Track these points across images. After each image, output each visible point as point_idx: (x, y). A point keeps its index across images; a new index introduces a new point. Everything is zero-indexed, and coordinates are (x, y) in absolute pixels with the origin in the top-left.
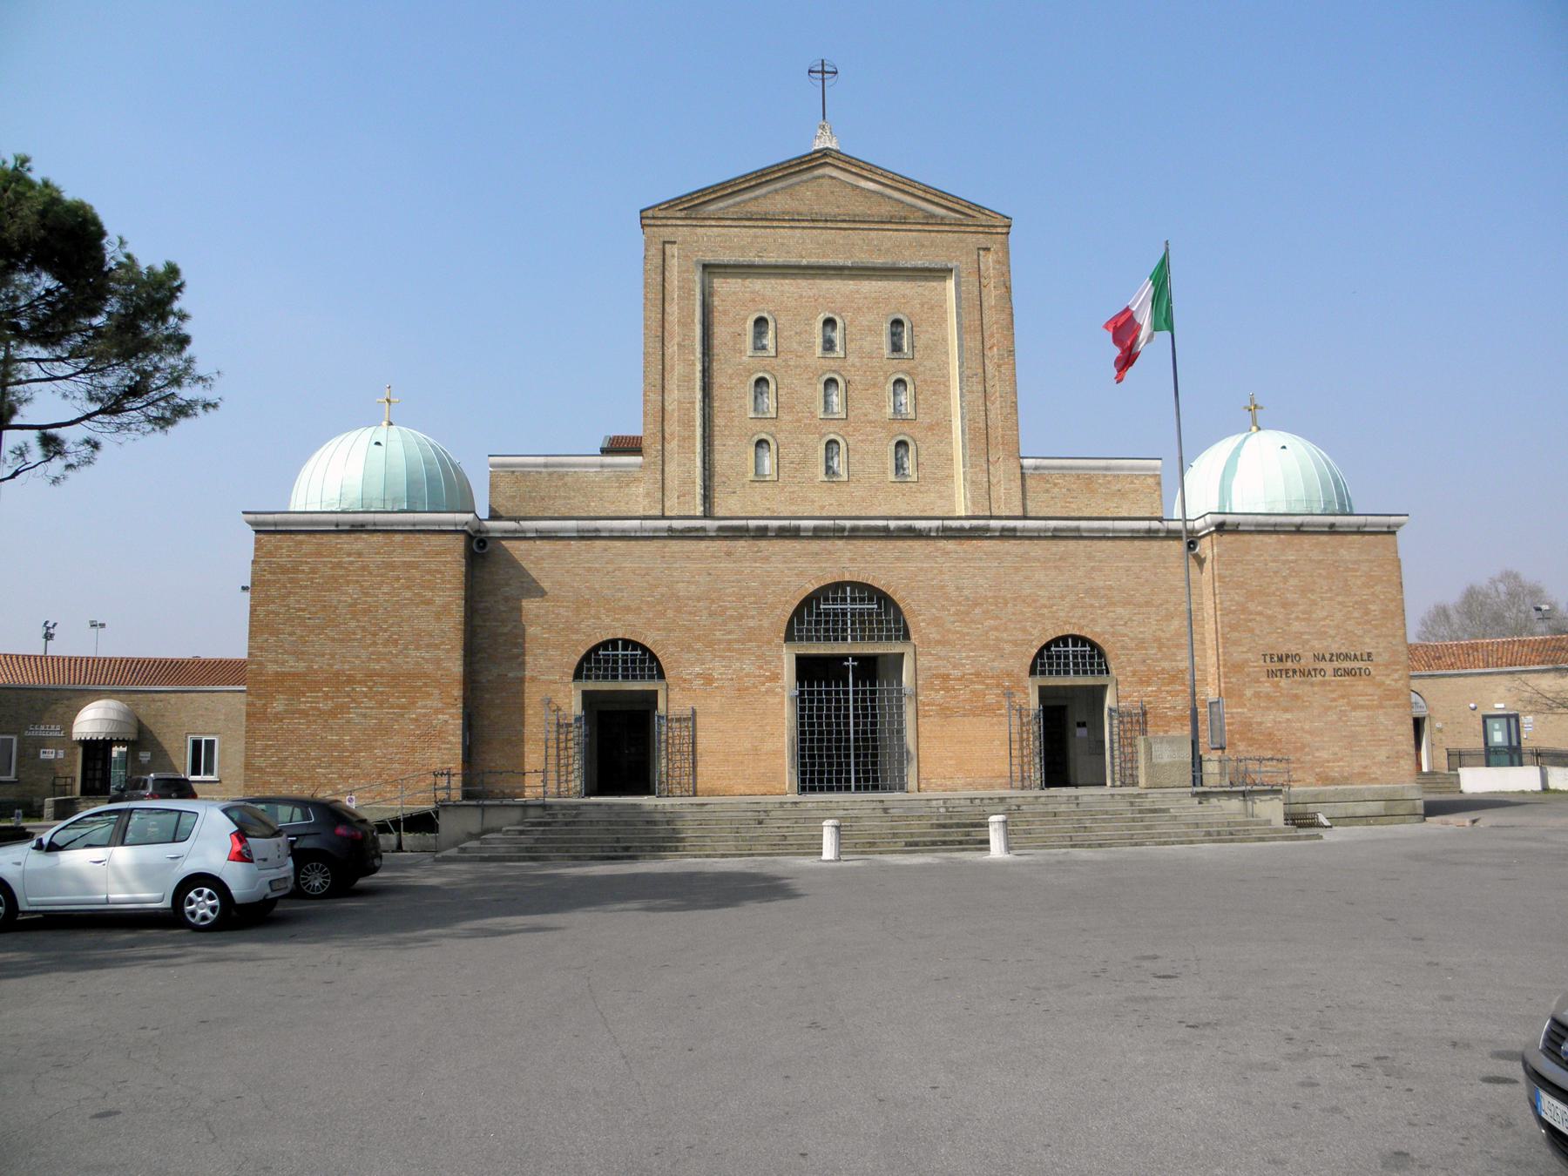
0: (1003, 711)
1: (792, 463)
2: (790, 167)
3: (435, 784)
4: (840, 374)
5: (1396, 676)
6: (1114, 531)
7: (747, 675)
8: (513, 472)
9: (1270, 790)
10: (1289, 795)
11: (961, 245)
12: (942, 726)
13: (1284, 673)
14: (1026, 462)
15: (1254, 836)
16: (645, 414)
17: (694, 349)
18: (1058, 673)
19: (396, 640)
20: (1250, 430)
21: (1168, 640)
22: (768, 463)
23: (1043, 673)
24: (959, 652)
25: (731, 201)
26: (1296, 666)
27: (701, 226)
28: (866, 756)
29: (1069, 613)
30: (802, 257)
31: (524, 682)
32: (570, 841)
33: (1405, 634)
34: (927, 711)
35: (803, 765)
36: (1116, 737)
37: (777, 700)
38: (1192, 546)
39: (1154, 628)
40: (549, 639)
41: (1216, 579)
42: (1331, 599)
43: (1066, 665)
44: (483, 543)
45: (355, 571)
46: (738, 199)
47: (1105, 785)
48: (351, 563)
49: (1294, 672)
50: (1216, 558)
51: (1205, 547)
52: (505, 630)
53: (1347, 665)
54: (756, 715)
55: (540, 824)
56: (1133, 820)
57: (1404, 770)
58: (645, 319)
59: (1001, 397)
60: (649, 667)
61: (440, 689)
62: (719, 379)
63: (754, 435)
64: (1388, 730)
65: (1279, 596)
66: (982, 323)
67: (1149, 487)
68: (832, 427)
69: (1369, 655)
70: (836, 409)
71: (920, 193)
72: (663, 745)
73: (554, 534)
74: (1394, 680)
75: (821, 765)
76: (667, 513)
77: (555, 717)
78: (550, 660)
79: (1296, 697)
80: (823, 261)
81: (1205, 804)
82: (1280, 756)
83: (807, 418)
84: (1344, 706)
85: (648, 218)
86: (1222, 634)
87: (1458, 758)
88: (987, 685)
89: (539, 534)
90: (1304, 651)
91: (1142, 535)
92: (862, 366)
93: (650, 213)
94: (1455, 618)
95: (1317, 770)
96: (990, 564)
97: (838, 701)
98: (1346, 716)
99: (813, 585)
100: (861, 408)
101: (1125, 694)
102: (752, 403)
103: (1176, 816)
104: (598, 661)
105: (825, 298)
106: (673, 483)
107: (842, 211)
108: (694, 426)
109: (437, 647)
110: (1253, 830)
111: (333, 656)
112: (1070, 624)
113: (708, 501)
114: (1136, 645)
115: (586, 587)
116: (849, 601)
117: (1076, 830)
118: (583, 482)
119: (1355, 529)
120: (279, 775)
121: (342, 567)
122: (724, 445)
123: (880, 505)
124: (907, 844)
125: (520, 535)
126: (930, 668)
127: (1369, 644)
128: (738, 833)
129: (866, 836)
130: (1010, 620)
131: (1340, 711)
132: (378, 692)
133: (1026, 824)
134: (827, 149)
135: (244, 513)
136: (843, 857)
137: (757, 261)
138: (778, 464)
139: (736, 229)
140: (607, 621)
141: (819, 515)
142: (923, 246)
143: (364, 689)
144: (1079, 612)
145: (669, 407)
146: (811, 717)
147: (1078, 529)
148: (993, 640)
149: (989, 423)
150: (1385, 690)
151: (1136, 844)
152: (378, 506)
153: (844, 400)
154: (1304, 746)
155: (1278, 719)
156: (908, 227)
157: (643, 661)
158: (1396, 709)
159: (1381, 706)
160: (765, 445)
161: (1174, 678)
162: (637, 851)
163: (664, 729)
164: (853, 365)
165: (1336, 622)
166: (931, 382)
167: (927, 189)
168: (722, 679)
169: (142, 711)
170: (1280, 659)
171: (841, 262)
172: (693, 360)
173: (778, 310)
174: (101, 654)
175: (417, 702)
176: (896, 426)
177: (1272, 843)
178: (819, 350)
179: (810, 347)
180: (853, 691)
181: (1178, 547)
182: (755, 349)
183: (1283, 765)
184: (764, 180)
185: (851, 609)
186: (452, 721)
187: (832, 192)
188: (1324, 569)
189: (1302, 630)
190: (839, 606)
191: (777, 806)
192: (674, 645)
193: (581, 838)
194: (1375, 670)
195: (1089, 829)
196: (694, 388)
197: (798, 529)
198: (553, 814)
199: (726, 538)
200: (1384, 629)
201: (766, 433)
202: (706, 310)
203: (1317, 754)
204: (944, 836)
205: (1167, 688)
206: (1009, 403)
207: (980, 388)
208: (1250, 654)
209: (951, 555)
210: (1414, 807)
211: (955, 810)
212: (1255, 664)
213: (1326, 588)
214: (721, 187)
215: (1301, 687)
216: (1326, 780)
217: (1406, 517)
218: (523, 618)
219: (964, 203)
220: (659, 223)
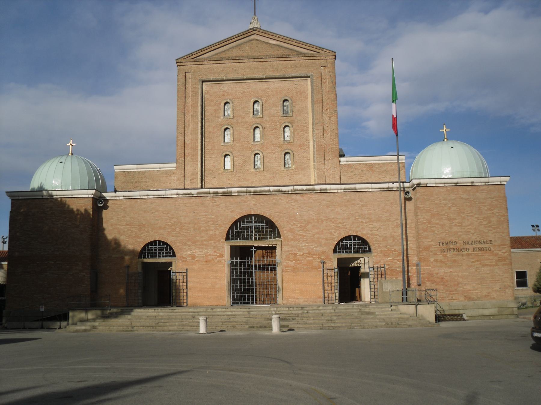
1: (240, 164)
4: (260, 125)
5: (504, 251)
7: (210, 255)
20: (444, 140)
23: (339, 252)
24: (301, 244)
26: (455, 247)
29: (351, 225)
30: (244, 75)
33: (509, 231)
37: (222, 265)
39: (391, 231)
43: (155, 253)
49: (454, 250)
53: (479, 246)
54: (213, 272)
63: (223, 152)
64: (500, 276)
65: (447, 215)
69: (491, 241)
71: (296, 44)
76: (186, 187)
79: (455, 261)
83: (246, 144)
88: (314, 258)
91: (385, 190)
93: (180, 60)
99: (238, 216)
100: (269, 139)
107: (261, 54)
108: (198, 150)
115: (143, 219)
122: (211, 157)
126: (288, 251)
127: (491, 236)
130: (325, 229)
131: (476, 267)
141: (251, 186)
142: (297, 67)
143: (53, 263)
146: (236, 272)
148: (317, 238)
150: (499, 257)
154: (458, 284)
155: (446, 272)
157: (166, 250)
158: (504, 266)
159: (497, 265)
165: (474, 227)
166: (300, 126)
168: (199, 257)
170: (447, 244)
172: (198, 122)
173: (234, 99)
178: (251, 115)
187: (257, 47)
188: (469, 203)
190: (257, 225)
194: (493, 248)
196: (198, 134)
200: (498, 229)
201: (229, 151)
203: (465, 287)
205: (397, 258)
208: (433, 242)
210: (513, 311)
213: (470, 211)
215: (457, 256)
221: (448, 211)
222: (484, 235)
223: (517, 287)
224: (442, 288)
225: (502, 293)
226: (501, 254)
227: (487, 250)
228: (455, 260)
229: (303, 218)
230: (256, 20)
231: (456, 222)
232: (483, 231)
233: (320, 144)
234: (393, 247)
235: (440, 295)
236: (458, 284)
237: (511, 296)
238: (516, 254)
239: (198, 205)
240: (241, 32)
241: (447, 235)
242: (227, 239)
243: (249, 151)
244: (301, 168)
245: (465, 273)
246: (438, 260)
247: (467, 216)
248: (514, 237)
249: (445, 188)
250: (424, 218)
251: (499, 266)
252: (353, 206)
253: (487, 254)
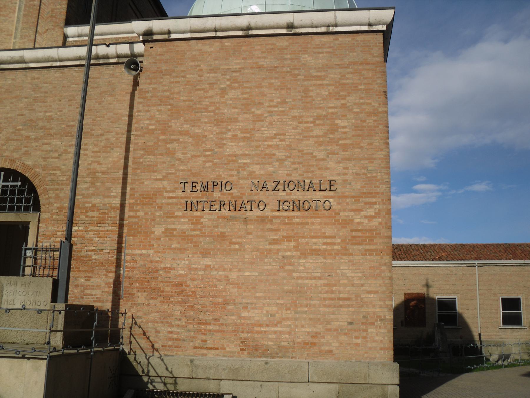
5: (371, 212)
21: (104, 173)
26: (226, 198)
42: (283, 113)
49: (222, 204)
53: (298, 195)
57: (375, 341)
64: (353, 285)
65: (214, 111)
69: (332, 183)
79: (222, 236)
84: (290, 250)
95: (242, 335)
98: (290, 264)
101: (48, 234)
144: (13, 145)
150: (352, 231)
154: (226, 303)
155: (193, 266)
159: (345, 252)
194: (339, 204)
200: (357, 150)
203: (244, 314)
208: (166, 182)
221: (217, 99)
222: (313, 166)
223: (503, 324)
224: (179, 313)
225: (357, 338)
226: (362, 220)
228: (221, 233)
231: (237, 127)
232: (312, 154)
234: (89, 200)
235: (171, 332)
236: (226, 303)
237: (381, 349)
238: (503, 268)
241: (207, 164)
245: (247, 274)
246: (175, 233)
248: (506, 244)
249: (217, 42)
250: (151, 118)
251: (351, 257)
252: (14, 100)
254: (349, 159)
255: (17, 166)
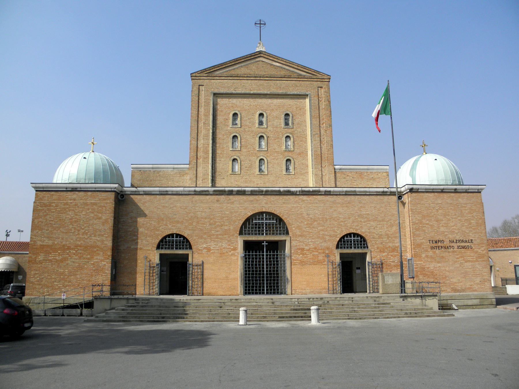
0: (326, 263)
1: (246, 167)
2: (247, 57)
3: (93, 289)
4: (265, 134)
5: (483, 249)
6: (369, 192)
7: (224, 248)
8: (140, 171)
9: (432, 295)
10: (440, 296)
11: (311, 86)
12: (302, 268)
13: (437, 247)
14: (336, 167)
15: (425, 315)
16: (190, 149)
17: (209, 125)
18: (348, 248)
19: (87, 233)
21: (391, 235)
22: (237, 167)
23: (341, 248)
24: (308, 239)
25: (225, 70)
26: (442, 245)
27: (213, 79)
28: (271, 280)
29: (352, 224)
31: (137, 250)
32: (141, 314)
34: (295, 263)
35: (246, 284)
36: (371, 273)
37: (236, 258)
38: (400, 198)
40: (147, 233)
41: (410, 210)
44: (123, 196)
45: (72, 206)
46: (227, 69)
47: (367, 292)
48: (71, 203)
49: (442, 247)
50: (410, 202)
51: (405, 198)
52: (131, 230)
53: (463, 244)
55: (131, 306)
56: (375, 307)
58: (191, 113)
59: (327, 142)
60: (186, 245)
61: (103, 252)
62: (219, 136)
63: (232, 157)
64: (480, 271)
65: (435, 217)
66: (319, 115)
67: (384, 176)
68: (262, 154)
69: (472, 240)
70: (263, 147)
71: (296, 67)
72: (191, 275)
73: (150, 193)
74: (482, 250)
75: (253, 284)
77: (148, 264)
78: (147, 241)
79: (443, 257)
80: (259, 92)
81: (406, 301)
82: (436, 281)
83: (252, 150)
85: (194, 76)
86: (413, 232)
87: (505, 281)
88: (319, 252)
89: (145, 193)
90: (446, 239)
92: (273, 131)
93: (194, 75)
94: (500, 231)
95: (452, 286)
96: (320, 205)
97: (260, 258)
98: (463, 265)
100: (273, 147)
102: (231, 145)
103: (393, 306)
104: (166, 242)
105: (259, 106)
106: (200, 175)
107: (266, 73)
108: (209, 153)
109: (103, 235)
110: (425, 312)
111: (62, 239)
112: (352, 228)
113: (213, 182)
114: (379, 237)
115: (162, 213)
116: (264, 219)
117: (351, 312)
118: (166, 174)
119: (465, 191)
120: (40, 285)
121: (67, 205)
122: (220, 161)
123: (280, 183)
124: (280, 317)
125: (138, 193)
126: (296, 246)
127: (471, 236)
128: (211, 311)
129: (263, 314)
130: (328, 227)
131: (461, 263)
132: (79, 253)
133: (330, 309)
134: (261, 51)
135: (31, 183)
136: (248, 323)
137: (234, 92)
138: (241, 168)
139: (226, 80)
140: (170, 226)
142: (297, 86)
143: (74, 252)
145: (199, 146)
146: (249, 265)
147: (355, 191)
148: (322, 235)
149: (322, 152)
150: (478, 254)
151: (376, 318)
152: (83, 181)
153: (266, 144)
154: (446, 277)
156: (291, 79)
157: (183, 242)
160: (236, 161)
161: (394, 250)
162: (167, 319)
163: (191, 269)
164: (270, 131)
167: (298, 65)
169: (20, 261)
171: (266, 92)
174: (21, 241)
175: (94, 257)
176: (286, 153)
177: (433, 318)
178: (257, 125)
179: (254, 124)
180: (266, 254)
181: (395, 198)
182: (233, 125)
183: (438, 284)
184: (237, 62)
185: (266, 222)
186: (107, 265)
189: (445, 231)
191: (229, 300)
192: (196, 236)
193: (146, 313)
195: (356, 312)
197: (245, 191)
198: (138, 302)
199: (217, 195)
200: (477, 230)
201: (236, 156)
202: (214, 111)
204: (296, 314)
205: (391, 254)
206: (330, 145)
207: (319, 139)
209: (305, 201)
211: (302, 303)
212: (426, 244)
214: (221, 65)
216: (456, 290)
217: (485, 186)
218: (138, 225)
219: (312, 70)
220: (197, 78)
221: (436, 213)
222: (465, 235)
227: (469, 248)
229: (309, 217)
230: (262, 45)
233: (317, 153)
239: (214, 202)
240: (229, 60)
242: (241, 233)
243: (255, 156)
244: (301, 173)
247: (452, 218)
250: (416, 219)
253: (469, 251)
254: (476, 233)
255: (358, 232)
